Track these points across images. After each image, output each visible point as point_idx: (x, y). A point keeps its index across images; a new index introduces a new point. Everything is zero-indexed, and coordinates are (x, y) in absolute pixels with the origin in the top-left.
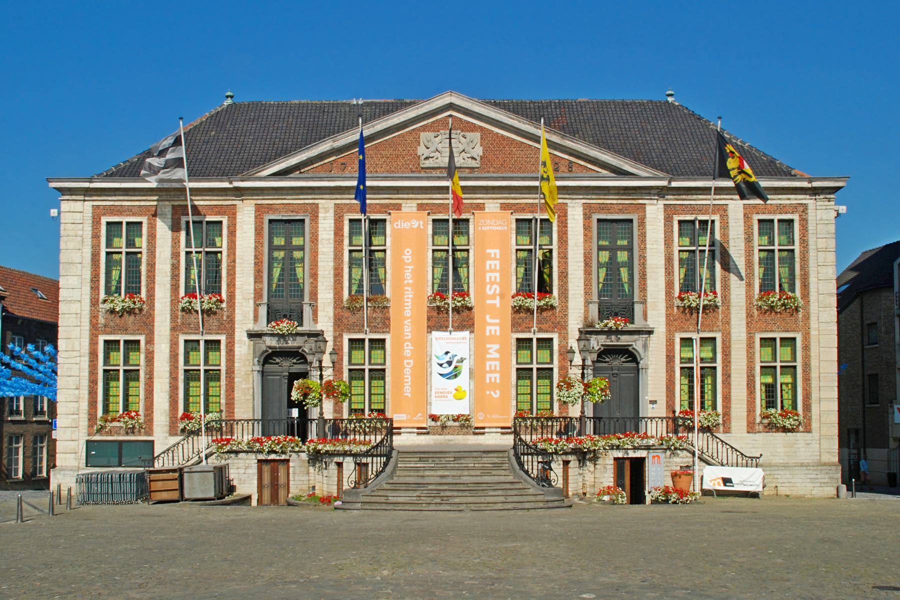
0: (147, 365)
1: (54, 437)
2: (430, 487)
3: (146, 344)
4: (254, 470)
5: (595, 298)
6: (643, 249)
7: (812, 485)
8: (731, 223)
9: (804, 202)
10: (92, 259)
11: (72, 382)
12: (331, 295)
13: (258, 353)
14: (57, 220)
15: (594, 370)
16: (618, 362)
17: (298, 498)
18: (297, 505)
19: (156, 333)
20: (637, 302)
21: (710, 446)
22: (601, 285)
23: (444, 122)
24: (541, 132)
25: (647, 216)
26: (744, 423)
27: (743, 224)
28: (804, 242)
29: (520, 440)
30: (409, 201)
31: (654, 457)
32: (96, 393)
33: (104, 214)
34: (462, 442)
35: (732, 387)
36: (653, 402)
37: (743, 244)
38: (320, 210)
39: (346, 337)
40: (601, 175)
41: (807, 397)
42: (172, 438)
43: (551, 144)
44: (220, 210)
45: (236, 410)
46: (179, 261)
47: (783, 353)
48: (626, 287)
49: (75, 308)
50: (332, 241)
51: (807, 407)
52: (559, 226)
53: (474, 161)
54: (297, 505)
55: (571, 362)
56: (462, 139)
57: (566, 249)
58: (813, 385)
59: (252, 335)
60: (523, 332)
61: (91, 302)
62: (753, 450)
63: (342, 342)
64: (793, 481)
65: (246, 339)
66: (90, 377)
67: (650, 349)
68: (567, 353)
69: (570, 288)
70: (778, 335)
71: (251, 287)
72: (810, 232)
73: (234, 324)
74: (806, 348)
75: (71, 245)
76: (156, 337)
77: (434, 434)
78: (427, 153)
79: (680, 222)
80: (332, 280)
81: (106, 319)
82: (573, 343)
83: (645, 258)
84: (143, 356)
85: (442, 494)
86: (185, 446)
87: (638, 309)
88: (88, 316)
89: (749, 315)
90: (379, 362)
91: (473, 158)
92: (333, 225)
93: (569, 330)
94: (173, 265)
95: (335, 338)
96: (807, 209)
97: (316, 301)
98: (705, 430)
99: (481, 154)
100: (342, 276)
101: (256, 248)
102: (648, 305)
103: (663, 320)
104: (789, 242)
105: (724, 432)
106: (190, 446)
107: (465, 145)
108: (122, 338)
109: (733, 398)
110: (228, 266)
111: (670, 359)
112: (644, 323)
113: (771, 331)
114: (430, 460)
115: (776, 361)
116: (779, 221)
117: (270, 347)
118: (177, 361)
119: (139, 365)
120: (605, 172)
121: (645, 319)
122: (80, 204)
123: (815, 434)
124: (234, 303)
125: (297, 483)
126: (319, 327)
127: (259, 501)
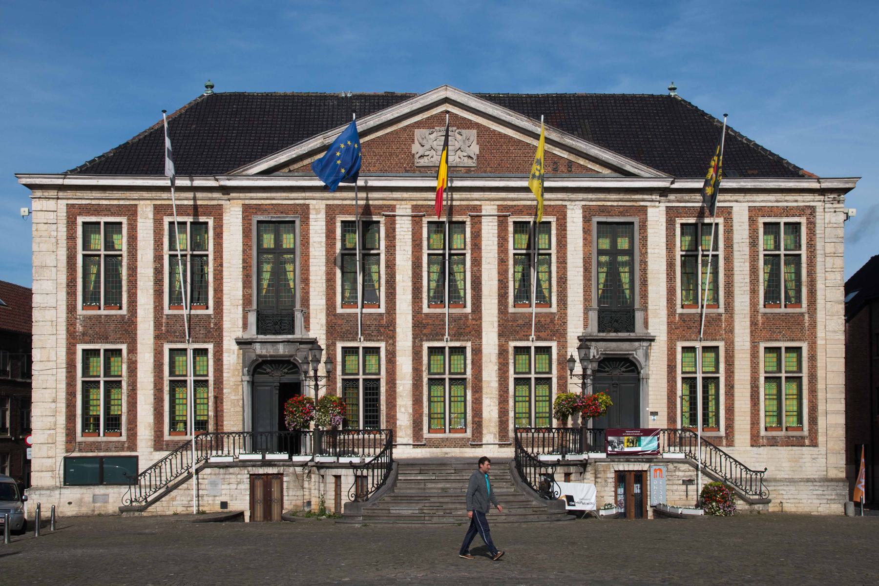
1: (28, 458)
2: (432, 500)
3: (128, 353)
4: (246, 486)
5: (594, 304)
6: (644, 254)
7: (819, 501)
8: (736, 227)
10: (68, 262)
11: (48, 395)
12: (324, 302)
13: (247, 363)
14: (27, 219)
15: (593, 380)
16: (618, 372)
17: (294, 513)
18: (292, 521)
19: (139, 341)
20: (638, 309)
21: (713, 460)
22: (600, 291)
23: (438, 120)
24: (540, 129)
25: (649, 219)
26: (748, 437)
27: (747, 227)
28: (811, 246)
29: (523, 451)
30: (403, 202)
31: (655, 470)
32: (75, 406)
33: (80, 214)
34: (458, 455)
35: (736, 398)
36: (654, 414)
37: (748, 249)
38: (311, 211)
39: (339, 345)
40: (601, 175)
41: (813, 409)
42: (158, 453)
43: (548, 141)
44: (120, 210)
45: (225, 423)
46: (162, 265)
47: (788, 362)
48: (627, 292)
49: (50, 315)
50: (324, 244)
51: (813, 420)
52: (557, 229)
53: (470, 160)
54: (292, 521)
55: (571, 371)
56: (458, 136)
57: (565, 254)
58: (819, 397)
61: (68, 309)
62: (757, 464)
63: (335, 350)
64: (799, 497)
65: (236, 347)
67: (651, 358)
68: (566, 363)
69: (569, 295)
70: (783, 345)
71: (239, 293)
72: (818, 236)
73: (222, 332)
74: (813, 358)
75: (44, 247)
76: (139, 345)
77: (430, 447)
79: (85, 224)
80: (324, 285)
81: (84, 326)
82: (573, 351)
83: (646, 263)
84: (125, 367)
85: (444, 507)
86: (174, 461)
88: (65, 324)
89: (753, 323)
90: (373, 371)
91: (469, 157)
92: (324, 227)
93: (568, 338)
94: (156, 269)
95: (328, 346)
97: (308, 308)
98: (706, 442)
99: (478, 152)
100: (335, 282)
101: (244, 251)
102: (649, 312)
103: (664, 328)
104: (796, 247)
105: (728, 445)
106: (179, 461)
107: (461, 143)
108: (102, 347)
109: (736, 410)
110: (215, 270)
111: (671, 368)
112: (645, 331)
113: (776, 340)
114: (431, 472)
115: (780, 372)
116: (785, 224)
119: (121, 376)
120: (606, 172)
122: (53, 202)
123: (822, 449)
124: (222, 310)
125: (291, 498)
126: (312, 335)
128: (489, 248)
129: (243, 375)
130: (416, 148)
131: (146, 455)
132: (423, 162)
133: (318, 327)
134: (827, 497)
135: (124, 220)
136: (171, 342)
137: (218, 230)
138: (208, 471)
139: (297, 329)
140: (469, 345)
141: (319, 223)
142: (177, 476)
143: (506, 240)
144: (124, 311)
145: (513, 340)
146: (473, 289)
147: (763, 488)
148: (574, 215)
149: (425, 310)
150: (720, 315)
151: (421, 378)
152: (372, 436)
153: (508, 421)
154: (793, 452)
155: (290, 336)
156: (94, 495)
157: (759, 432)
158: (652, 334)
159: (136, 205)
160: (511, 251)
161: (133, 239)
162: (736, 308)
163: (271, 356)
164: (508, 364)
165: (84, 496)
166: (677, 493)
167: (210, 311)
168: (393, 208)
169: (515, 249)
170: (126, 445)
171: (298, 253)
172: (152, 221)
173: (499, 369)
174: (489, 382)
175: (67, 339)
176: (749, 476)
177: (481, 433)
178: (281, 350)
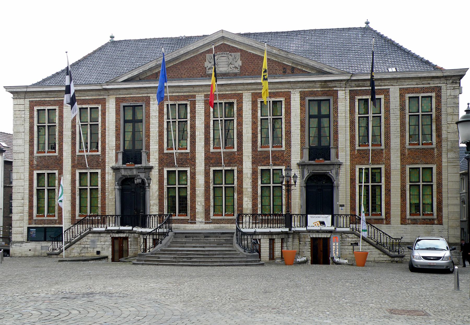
3: (59, 175)
33: (36, 106)
36: (342, 206)
51: (440, 209)
59: (116, 169)
61: (30, 153)
65: (111, 171)
67: (340, 175)
71: (114, 143)
74: (439, 174)
87: (333, 152)
89: (402, 154)
94: (72, 132)
108: (46, 172)
117: (124, 176)
118: (75, 184)
123: (445, 226)
126: (151, 164)
138: (90, 235)
140: (235, 168)
144: (57, 154)
148: (295, 97)
150: (382, 150)
151: (209, 187)
154: (427, 228)
155: (139, 165)
157: (406, 216)
158: (341, 161)
162: (391, 146)
163: (129, 176)
164: (257, 178)
166: (347, 250)
167: (99, 153)
168: (194, 96)
174: (247, 188)
175: (29, 168)
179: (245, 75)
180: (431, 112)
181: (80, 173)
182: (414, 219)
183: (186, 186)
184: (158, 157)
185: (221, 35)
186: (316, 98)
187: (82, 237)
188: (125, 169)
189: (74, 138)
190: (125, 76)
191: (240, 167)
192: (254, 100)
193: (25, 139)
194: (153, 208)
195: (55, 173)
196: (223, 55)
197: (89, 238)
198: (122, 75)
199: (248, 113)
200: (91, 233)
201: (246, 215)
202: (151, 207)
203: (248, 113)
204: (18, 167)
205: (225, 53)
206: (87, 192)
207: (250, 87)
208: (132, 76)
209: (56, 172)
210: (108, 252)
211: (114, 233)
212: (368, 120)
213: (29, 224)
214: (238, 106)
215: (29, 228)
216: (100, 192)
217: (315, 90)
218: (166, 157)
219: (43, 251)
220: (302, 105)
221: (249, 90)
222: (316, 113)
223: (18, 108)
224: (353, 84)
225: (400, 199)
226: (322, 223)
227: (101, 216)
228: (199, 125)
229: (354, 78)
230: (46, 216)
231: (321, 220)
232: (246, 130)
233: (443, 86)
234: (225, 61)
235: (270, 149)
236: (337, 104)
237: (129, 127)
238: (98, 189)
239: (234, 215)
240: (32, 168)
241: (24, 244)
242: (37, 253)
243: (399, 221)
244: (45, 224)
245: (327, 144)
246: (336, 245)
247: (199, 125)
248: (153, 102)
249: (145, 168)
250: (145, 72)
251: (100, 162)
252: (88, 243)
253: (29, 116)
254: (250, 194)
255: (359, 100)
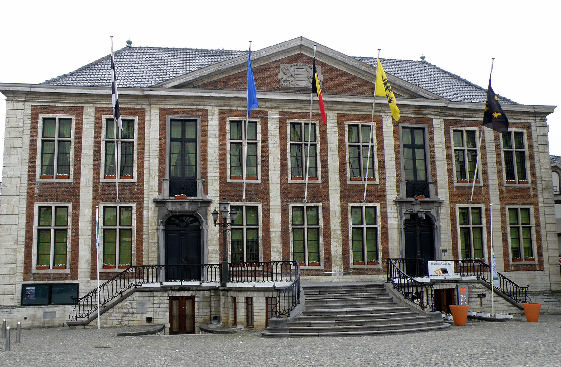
0: (73, 226)
3: (73, 209)
9: (529, 121)
10: (30, 145)
33: (41, 112)
36: (445, 251)
44: (70, 110)
46: (100, 148)
51: (540, 254)
57: (383, 146)
59: (157, 203)
60: (356, 202)
61: (29, 177)
65: (152, 206)
66: (26, 235)
67: (441, 215)
70: (519, 206)
71: (156, 168)
72: (534, 140)
74: (537, 215)
78: (285, 77)
79: (44, 119)
83: (434, 154)
87: (432, 187)
89: (501, 193)
92: (218, 124)
94: (95, 150)
96: (530, 126)
106: (114, 287)
108: (53, 205)
112: (436, 196)
113: (515, 204)
117: (171, 212)
121: (437, 194)
123: (547, 272)
126: (209, 197)
127: (171, 328)
128: (332, 141)
129: (158, 225)
130: (280, 75)
131: (85, 284)
132: (286, 85)
133: (214, 192)
134: (552, 303)
135: (73, 117)
136: (105, 202)
137: (141, 125)
138: (137, 294)
139: (199, 193)
140: (320, 205)
141: (214, 121)
142: (112, 298)
143: (344, 136)
144: (71, 180)
145: (351, 202)
146: (323, 167)
147: (527, 298)
148: (387, 122)
149: (290, 181)
150: (481, 187)
151: (288, 228)
152: (253, 268)
153: (349, 257)
154: (530, 275)
155: (193, 198)
156: (44, 313)
157: (509, 262)
158: (441, 199)
159: (83, 107)
160: (347, 144)
161: (79, 130)
162: (490, 183)
163: (179, 212)
164: (348, 218)
165: (37, 313)
166: (474, 304)
167: (135, 180)
168: (266, 113)
169: (349, 142)
170: (70, 276)
171: (199, 141)
172: (94, 118)
173: (342, 222)
174: (335, 230)
175: (28, 199)
176: (518, 290)
177: (330, 266)
178: (187, 208)
179: (328, 92)
180: (315, 141)
181: (105, 207)
182: (517, 265)
183: (257, 227)
184: (218, 188)
185: (299, 43)
186: (410, 126)
187: (123, 298)
188: (173, 202)
189: (97, 158)
190: (176, 80)
191: (326, 203)
192: (340, 122)
193: (23, 158)
194: (212, 254)
195: (67, 207)
196: (301, 67)
197: (135, 298)
198: (171, 80)
199: (333, 138)
200: (139, 291)
201: (211, 266)
202: (210, 255)
203: (333, 138)
204: (8, 198)
205: (304, 64)
206: (118, 235)
207: (334, 106)
208: (185, 81)
209: (70, 205)
210: (163, 319)
211: (173, 290)
212: (464, 153)
213: (24, 280)
214: (322, 129)
215: (24, 286)
216: (134, 234)
217: (409, 116)
218: (229, 189)
219: (47, 319)
220: (396, 132)
221: (334, 110)
222: (179, 136)
223: (13, 114)
224: (447, 112)
225: (502, 243)
226: (445, 271)
227: (136, 267)
228: (274, 149)
229: (450, 106)
230: (51, 268)
231: (443, 267)
232: (331, 157)
233: (532, 122)
234: (304, 73)
235: (307, 182)
236: (433, 133)
237: (177, 147)
238: (132, 229)
239: (320, 265)
240: (32, 199)
241: (15, 310)
242: (36, 323)
243: (503, 268)
244: (49, 279)
245: (193, 175)
246: (464, 298)
247: (274, 149)
248: (211, 117)
249: (201, 202)
250: (201, 78)
251: (135, 193)
252: (133, 306)
253: (30, 125)
254: (340, 238)
255: (231, 122)
